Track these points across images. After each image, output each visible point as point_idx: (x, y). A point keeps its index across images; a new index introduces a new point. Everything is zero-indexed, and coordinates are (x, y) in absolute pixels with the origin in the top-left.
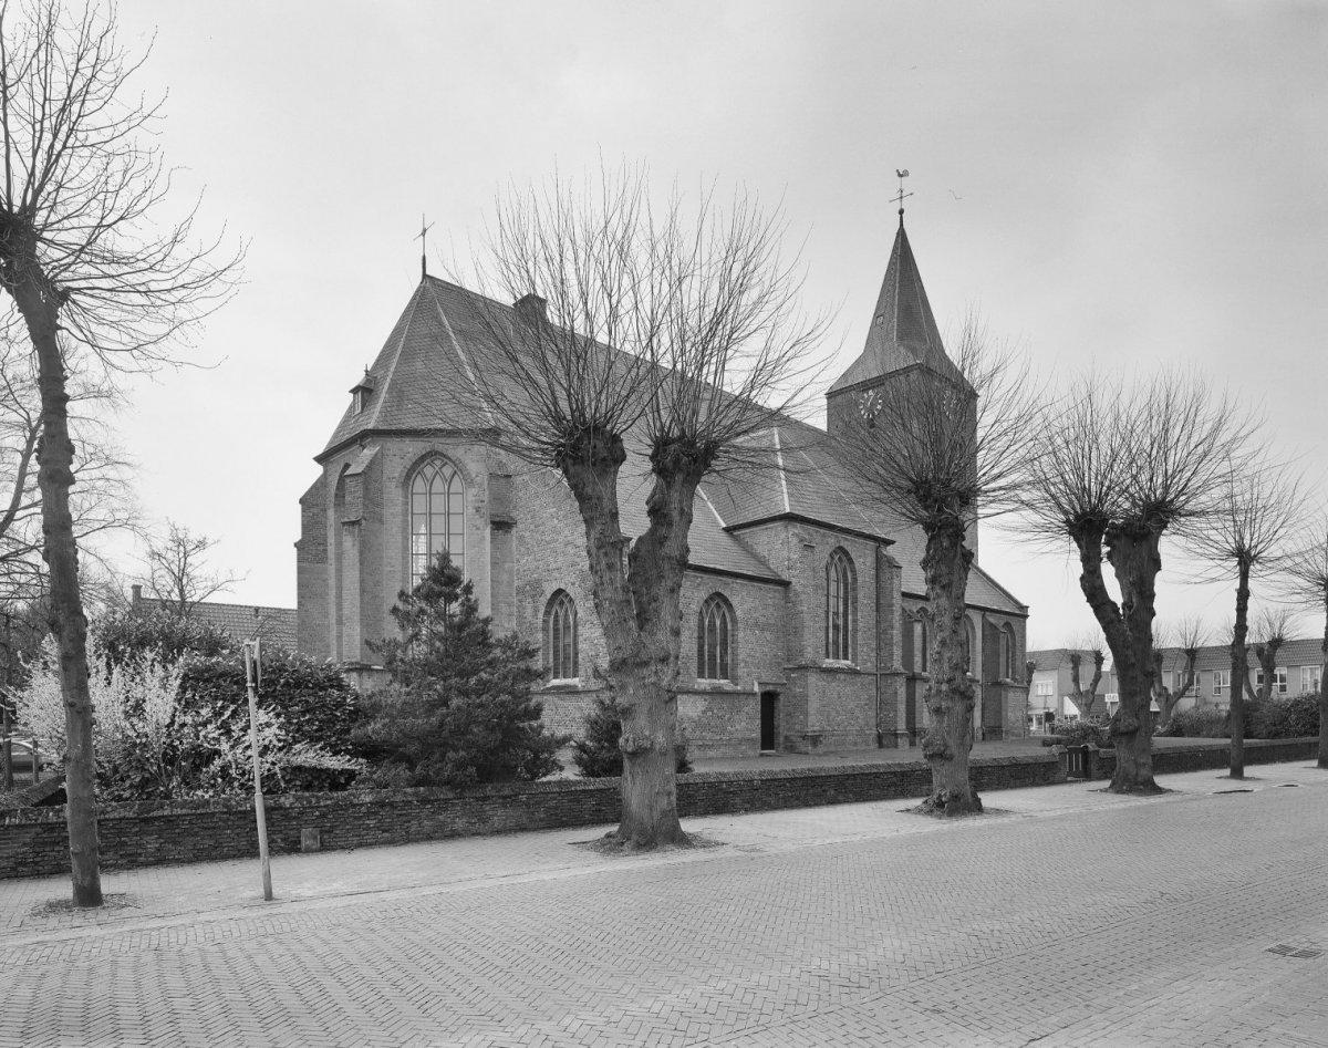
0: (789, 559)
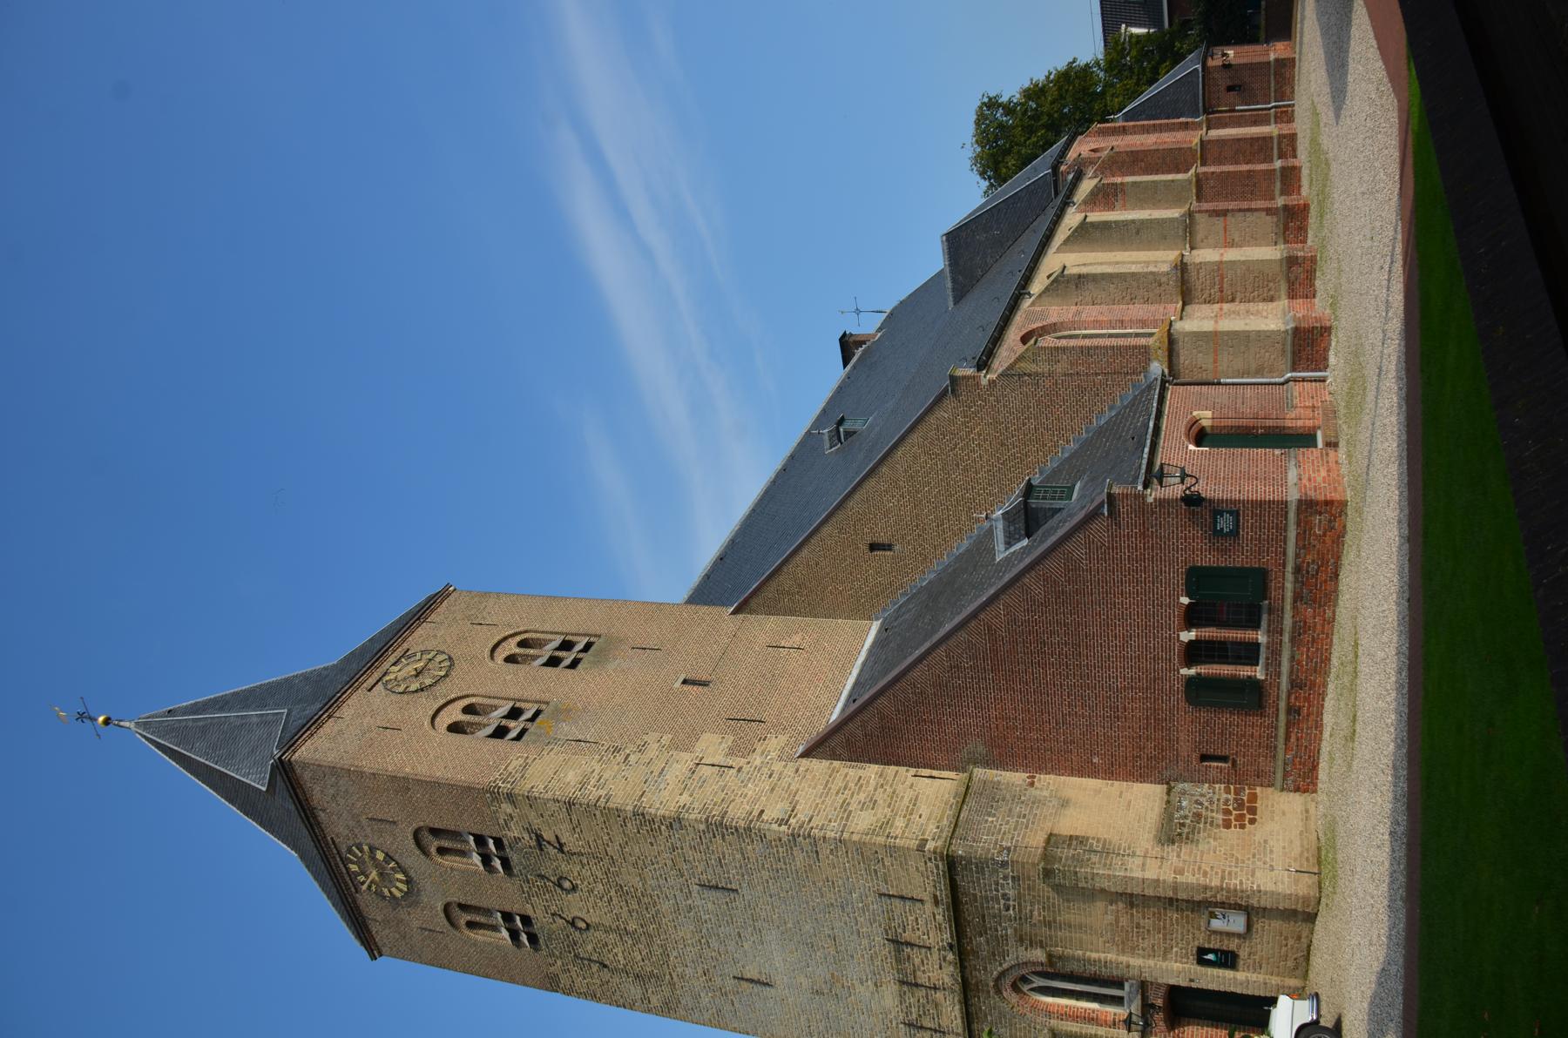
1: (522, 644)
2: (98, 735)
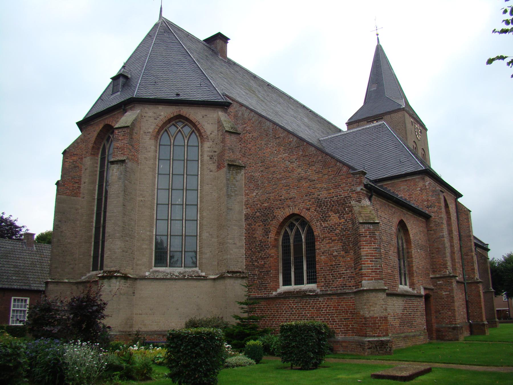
0: (428, 201)
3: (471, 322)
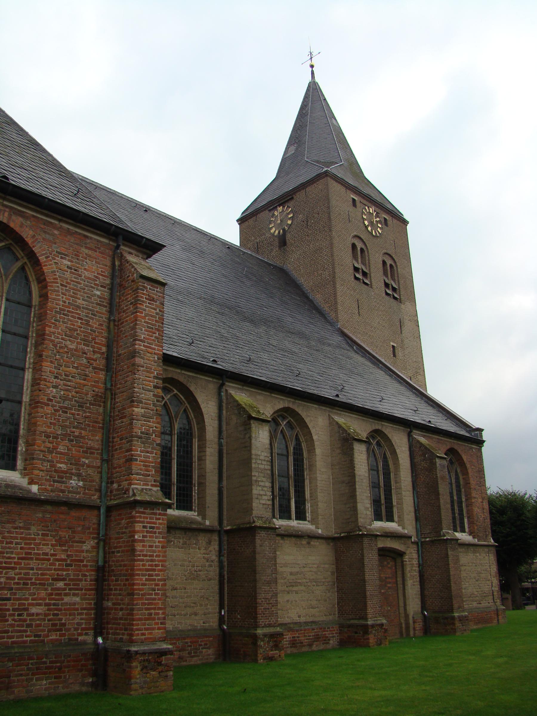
1: (391, 266)
2: (319, 53)
3: (426, 613)
